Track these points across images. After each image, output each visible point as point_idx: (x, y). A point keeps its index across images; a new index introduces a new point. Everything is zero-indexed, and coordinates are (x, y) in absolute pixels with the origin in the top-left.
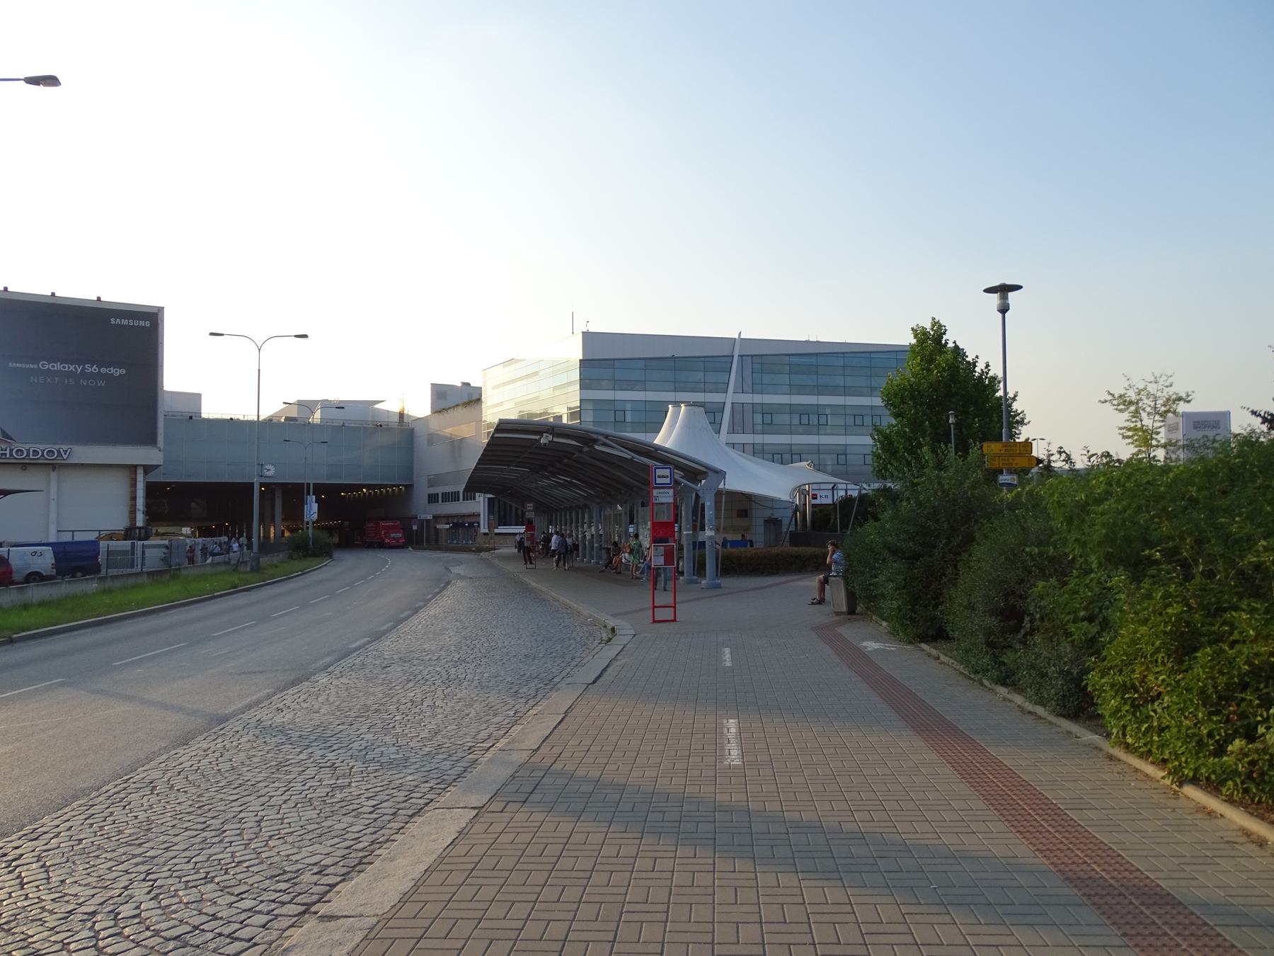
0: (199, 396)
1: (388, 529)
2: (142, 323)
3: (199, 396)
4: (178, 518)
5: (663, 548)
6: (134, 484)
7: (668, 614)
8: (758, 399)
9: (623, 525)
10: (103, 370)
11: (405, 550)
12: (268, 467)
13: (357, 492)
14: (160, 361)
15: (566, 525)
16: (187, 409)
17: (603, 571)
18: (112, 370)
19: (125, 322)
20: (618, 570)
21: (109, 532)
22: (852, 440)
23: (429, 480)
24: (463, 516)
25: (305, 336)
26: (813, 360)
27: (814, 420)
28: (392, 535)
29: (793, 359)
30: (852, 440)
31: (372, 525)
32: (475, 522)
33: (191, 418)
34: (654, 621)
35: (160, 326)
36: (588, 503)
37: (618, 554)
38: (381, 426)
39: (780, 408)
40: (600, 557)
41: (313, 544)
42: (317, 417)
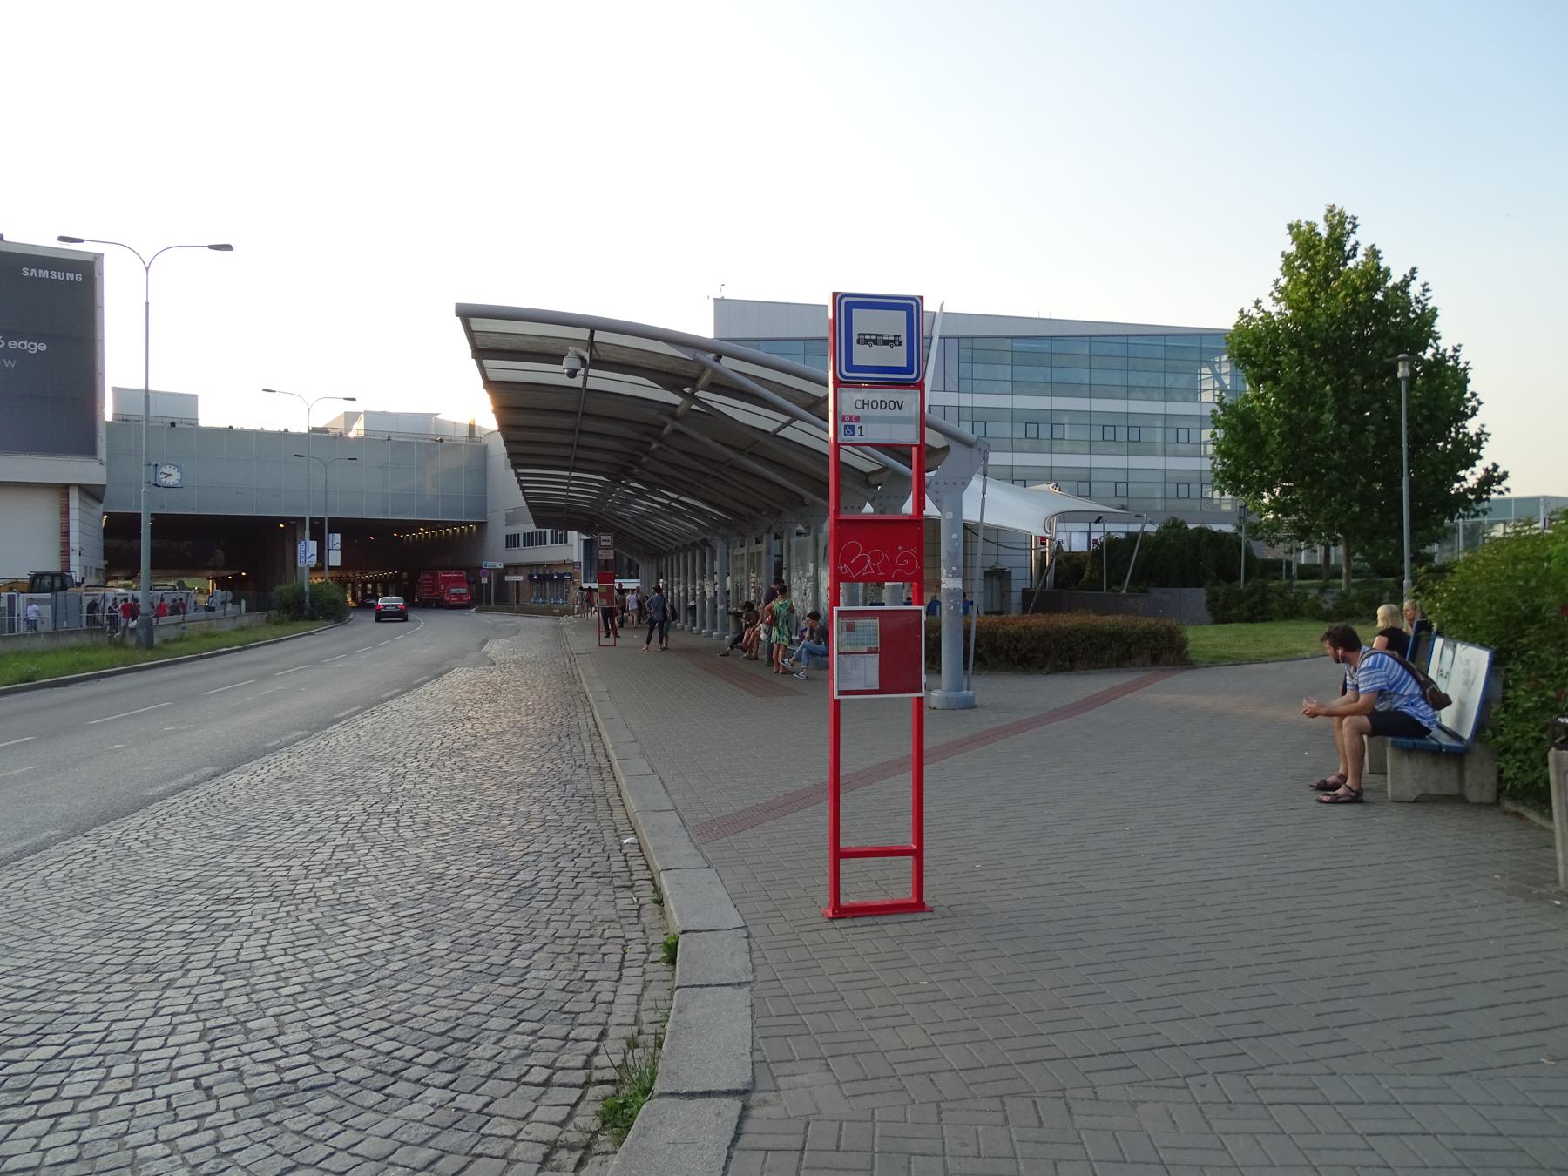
0: (195, 397)
1: (447, 581)
2: (70, 277)
3: (195, 397)
4: (193, 565)
5: (876, 622)
6: (65, 514)
7: (892, 880)
8: (966, 400)
9: (764, 572)
10: (12, 344)
11: (466, 612)
12: (167, 470)
13: (410, 534)
14: (98, 333)
15: (679, 576)
16: (174, 414)
17: (727, 654)
18: (26, 345)
19: (44, 274)
20: (753, 654)
21: (8, 581)
22: (1098, 461)
23: (508, 516)
24: (550, 565)
25: (228, 247)
26: (1045, 346)
27: (1045, 432)
28: (453, 591)
29: (1018, 345)
30: (1098, 461)
31: (428, 576)
32: (565, 574)
33: (173, 425)
34: (841, 912)
35: (98, 283)
36: (708, 537)
37: (753, 625)
38: (441, 441)
39: (995, 414)
40: (726, 627)
41: (310, 602)
42: (357, 430)
